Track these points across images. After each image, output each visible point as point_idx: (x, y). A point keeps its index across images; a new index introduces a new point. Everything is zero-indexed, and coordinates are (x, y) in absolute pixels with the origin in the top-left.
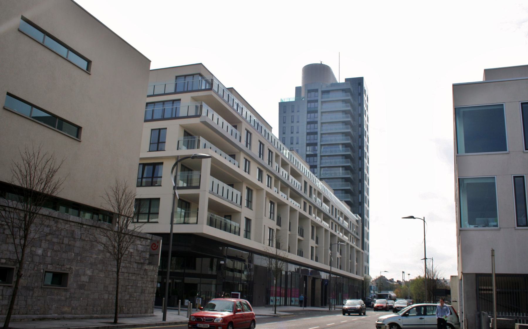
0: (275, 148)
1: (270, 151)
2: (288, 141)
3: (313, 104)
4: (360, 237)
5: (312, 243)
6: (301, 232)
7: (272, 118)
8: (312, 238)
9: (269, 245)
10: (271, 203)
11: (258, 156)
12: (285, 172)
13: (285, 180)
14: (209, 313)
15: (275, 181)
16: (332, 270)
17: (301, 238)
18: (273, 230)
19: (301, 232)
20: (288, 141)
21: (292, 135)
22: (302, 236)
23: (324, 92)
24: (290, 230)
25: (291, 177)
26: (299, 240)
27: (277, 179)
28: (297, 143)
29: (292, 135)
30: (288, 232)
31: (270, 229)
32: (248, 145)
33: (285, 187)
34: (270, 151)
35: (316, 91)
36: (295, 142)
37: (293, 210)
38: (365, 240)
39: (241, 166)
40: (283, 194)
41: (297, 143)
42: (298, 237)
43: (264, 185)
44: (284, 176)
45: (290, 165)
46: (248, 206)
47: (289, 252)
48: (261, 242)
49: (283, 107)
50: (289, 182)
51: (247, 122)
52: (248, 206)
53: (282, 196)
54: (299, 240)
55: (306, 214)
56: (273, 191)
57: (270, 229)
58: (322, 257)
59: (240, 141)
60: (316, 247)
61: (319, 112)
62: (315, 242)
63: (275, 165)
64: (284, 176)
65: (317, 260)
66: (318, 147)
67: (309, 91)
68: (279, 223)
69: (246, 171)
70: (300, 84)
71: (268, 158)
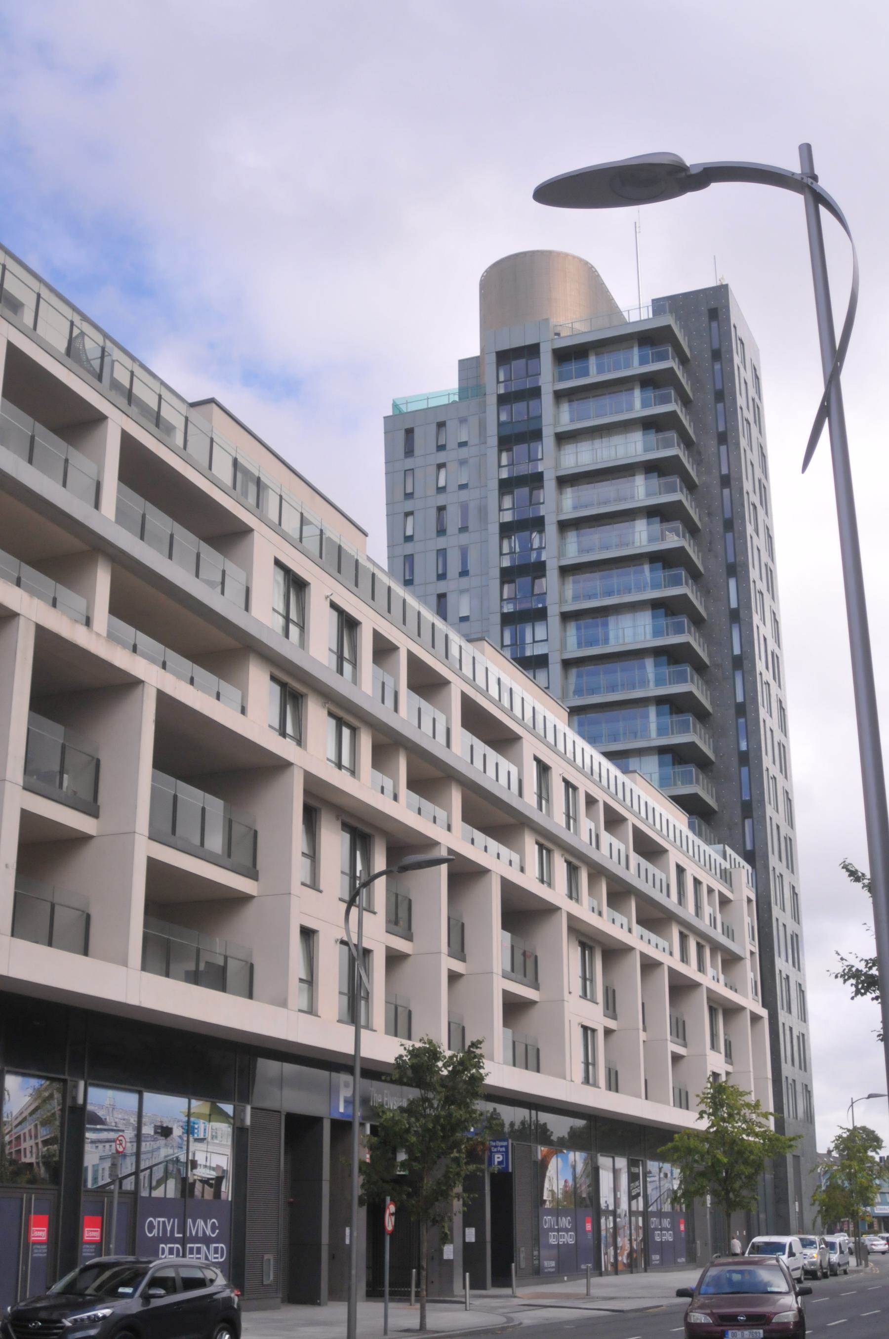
0: (602, 788)
1: (568, 784)
2: (426, 567)
3: (519, 408)
4: (746, 945)
5: (716, 1062)
6: (680, 1030)
7: (357, 484)
8: (714, 1046)
9: (587, 1081)
10: (583, 946)
11: (564, 825)
12: (617, 844)
13: (619, 870)
14: (690, 1278)
15: (590, 877)
16: (366, 1052)
17: (458, 966)
18: (594, 1031)
19: (680, 1030)
20: (426, 567)
21: (442, 542)
22: (614, 1017)
23: (563, 356)
24: (645, 1030)
25: (634, 858)
26: (454, 977)
27: (597, 872)
28: (464, 573)
29: (442, 542)
30: (642, 1036)
31: (585, 1029)
32: (347, 667)
33: (619, 893)
34: (568, 784)
35: (533, 351)
36: (454, 567)
37: (649, 966)
38: (781, 964)
39: (527, 868)
40: (504, 850)
41: (464, 573)
42: (450, 964)
43: (556, 894)
44: (503, 780)
45: (632, 820)
46: (584, 996)
47: (646, 1098)
48: (565, 1078)
49: (406, 434)
50: (631, 876)
51: (537, 736)
52: (584, 996)
53: (619, 927)
54: (454, 977)
55: (690, 971)
56: (584, 911)
57: (585, 1029)
58: (636, 1072)
59: (396, 709)
60: (608, 1032)
61: (548, 433)
62: (722, 1056)
63: (586, 825)
64: (503, 780)
65: (613, 1084)
66: (551, 582)
67: (504, 357)
68: (611, 1007)
69: (339, 766)
70: (473, 350)
71: (564, 810)
